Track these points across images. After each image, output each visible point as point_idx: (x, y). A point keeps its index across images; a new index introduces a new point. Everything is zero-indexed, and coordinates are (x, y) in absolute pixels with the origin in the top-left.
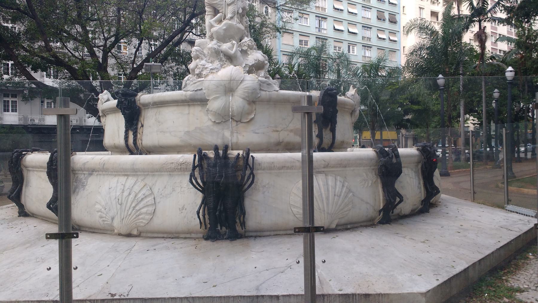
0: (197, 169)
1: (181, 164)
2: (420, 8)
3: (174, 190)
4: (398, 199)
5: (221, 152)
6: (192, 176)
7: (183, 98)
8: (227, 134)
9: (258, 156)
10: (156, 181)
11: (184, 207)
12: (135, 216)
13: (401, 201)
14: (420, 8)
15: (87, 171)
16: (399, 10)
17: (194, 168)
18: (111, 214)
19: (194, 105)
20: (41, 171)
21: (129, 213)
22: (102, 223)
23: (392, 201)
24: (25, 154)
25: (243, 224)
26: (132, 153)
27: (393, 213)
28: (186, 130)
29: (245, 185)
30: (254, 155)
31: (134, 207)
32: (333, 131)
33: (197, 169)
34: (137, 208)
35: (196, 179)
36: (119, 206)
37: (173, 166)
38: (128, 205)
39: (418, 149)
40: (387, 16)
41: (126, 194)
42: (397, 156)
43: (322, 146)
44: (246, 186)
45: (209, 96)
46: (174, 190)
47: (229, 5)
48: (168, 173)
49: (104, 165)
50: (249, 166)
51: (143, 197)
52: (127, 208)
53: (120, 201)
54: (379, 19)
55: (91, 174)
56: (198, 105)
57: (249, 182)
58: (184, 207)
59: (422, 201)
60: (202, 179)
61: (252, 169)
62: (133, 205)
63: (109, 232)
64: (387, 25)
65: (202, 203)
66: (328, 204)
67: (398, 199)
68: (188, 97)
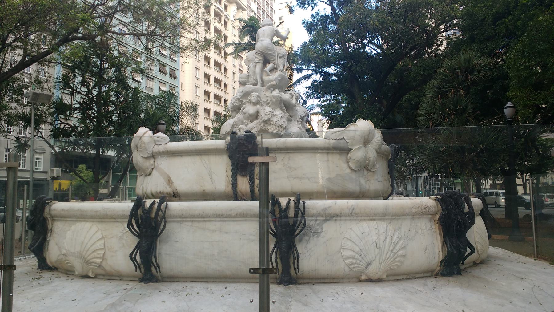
1: (425, 208)
2: (197, 68)
3: (417, 232)
6: (130, 225)
7: (327, 145)
8: (362, 181)
10: (401, 225)
11: (426, 248)
12: (392, 259)
13: (472, 252)
14: (197, 68)
15: (322, 216)
16: (179, 67)
18: (368, 259)
19: (333, 153)
20: (108, 222)
21: (387, 257)
22: (347, 269)
25: (297, 268)
28: (328, 176)
29: (297, 230)
30: (308, 202)
31: (392, 251)
34: (395, 251)
35: (133, 228)
36: (377, 251)
37: (419, 210)
38: (387, 248)
39: (436, 200)
40: (167, 69)
41: (382, 238)
44: (297, 232)
45: (352, 145)
46: (417, 232)
47: (280, 57)
48: (410, 217)
49: (353, 209)
50: (162, 211)
51: (398, 240)
52: (385, 253)
53: (378, 246)
54: (160, 71)
55: (326, 220)
56: (337, 153)
58: (426, 248)
60: (275, 226)
62: (391, 248)
63: (345, 280)
64: (167, 78)
66: (89, 256)
67: (469, 251)
68: (331, 145)
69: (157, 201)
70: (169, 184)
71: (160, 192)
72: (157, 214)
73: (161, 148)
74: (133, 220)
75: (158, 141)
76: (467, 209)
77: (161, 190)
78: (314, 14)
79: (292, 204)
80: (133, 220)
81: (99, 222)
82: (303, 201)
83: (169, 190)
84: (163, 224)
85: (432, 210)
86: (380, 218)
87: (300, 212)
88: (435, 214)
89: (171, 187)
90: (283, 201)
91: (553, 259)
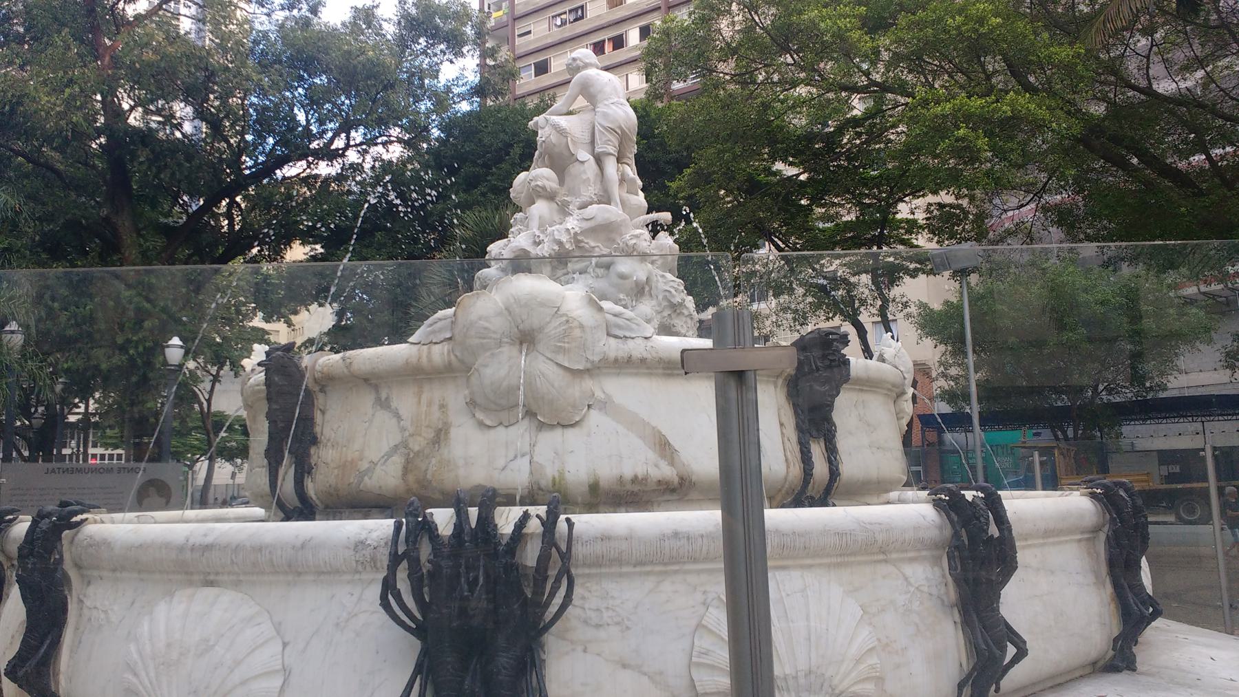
0: (405, 564)
4: (1011, 650)
5: (473, 512)
6: (389, 586)
9: (587, 523)
13: (1022, 653)
17: (395, 560)
20: (859, 563)
23: (998, 652)
24: (11, 521)
26: (289, 515)
27: (997, 690)
29: (548, 604)
32: (831, 451)
33: (405, 564)
42: (1001, 519)
43: (810, 492)
50: (558, 549)
57: (558, 600)
59: (1115, 640)
61: (566, 556)
65: (418, 669)
67: (1011, 650)
69: (542, 510)
70: (663, 456)
71: (635, 480)
72: (544, 559)
73: (636, 348)
74: (390, 597)
75: (619, 327)
76: (994, 530)
77: (640, 471)
78: (608, 47)
79: (534, 526)
80: (390, 597)
81: (829, 566)
82: (568, 520)
83: (666, 471)
84: (558, 600)
85: (933, 534)
86: (834, 560)
87: (560, 557)
88: (1096, 530)
89: (672, 464)
90: (506, 519)
91: (1231, 627)
